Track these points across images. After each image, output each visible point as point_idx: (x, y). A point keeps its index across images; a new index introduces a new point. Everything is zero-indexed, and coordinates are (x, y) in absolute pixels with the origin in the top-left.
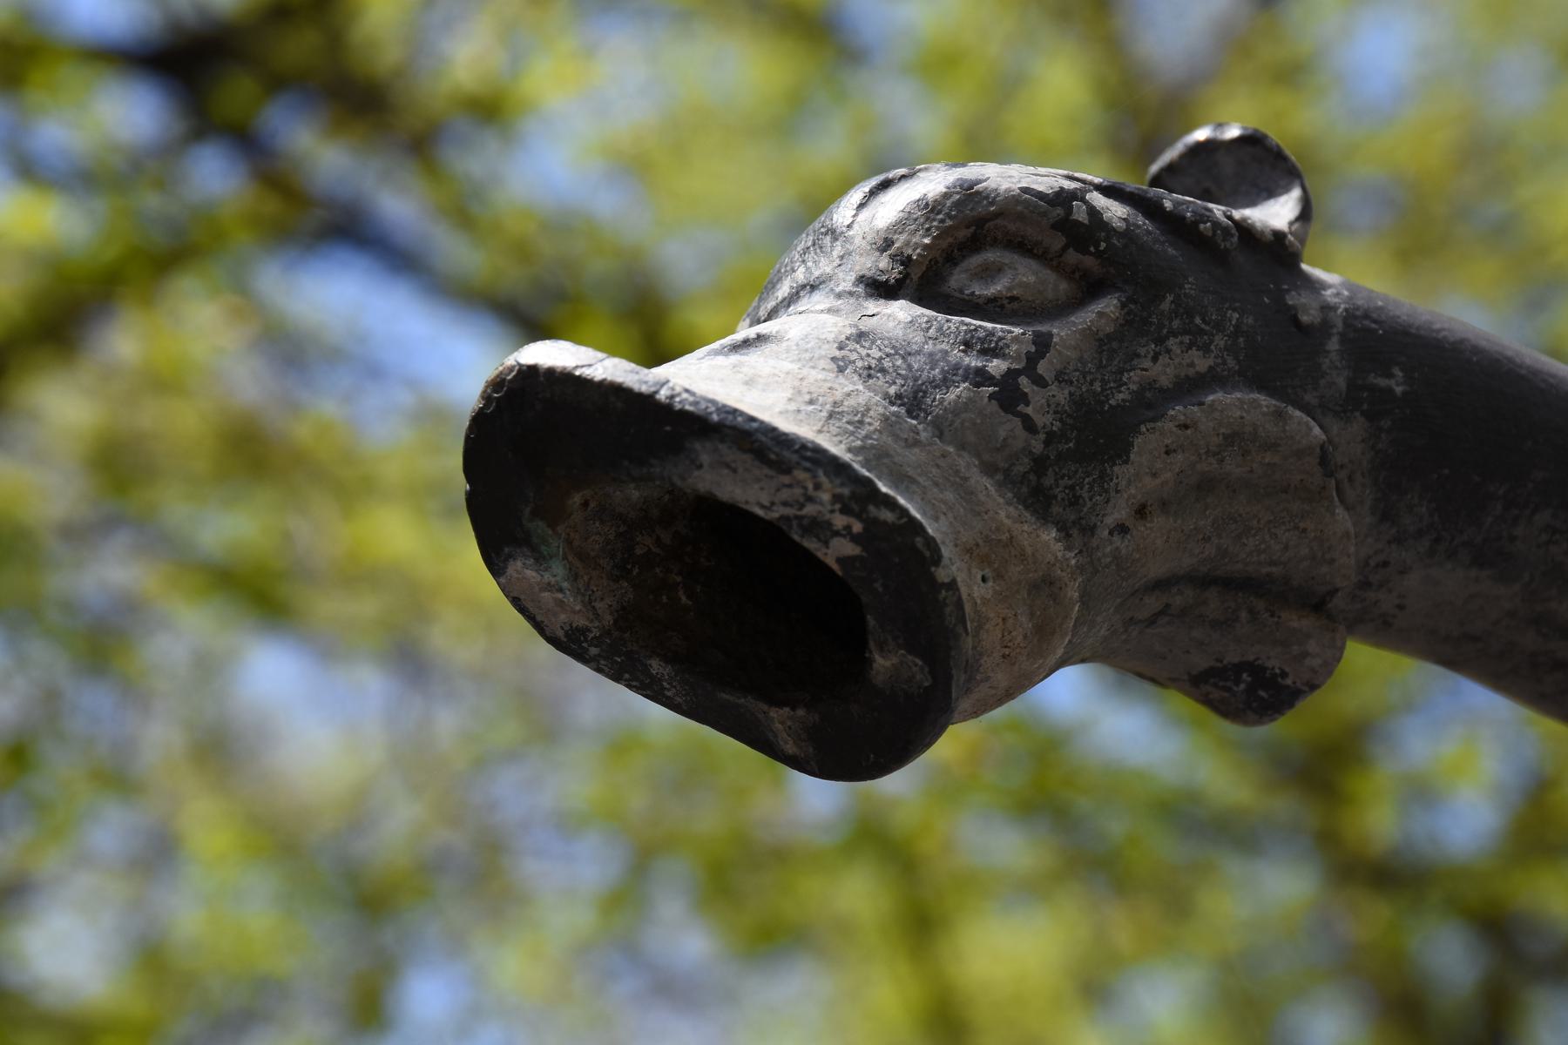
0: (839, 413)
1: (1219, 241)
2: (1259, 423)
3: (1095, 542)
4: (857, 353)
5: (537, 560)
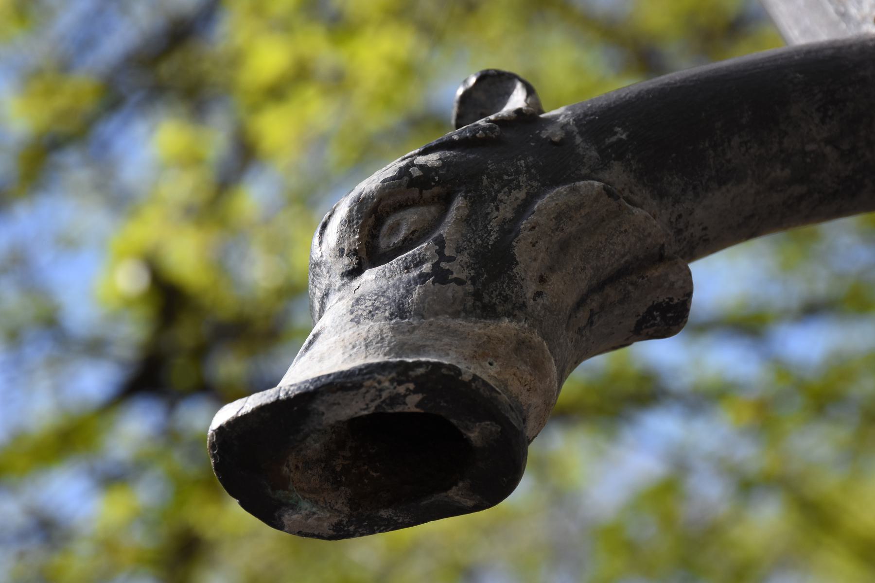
0: (369, 342)
1: (491, 135)
2: (566, 201)
3: (530, 310)
4: (361, 310)
5: (292, 508)
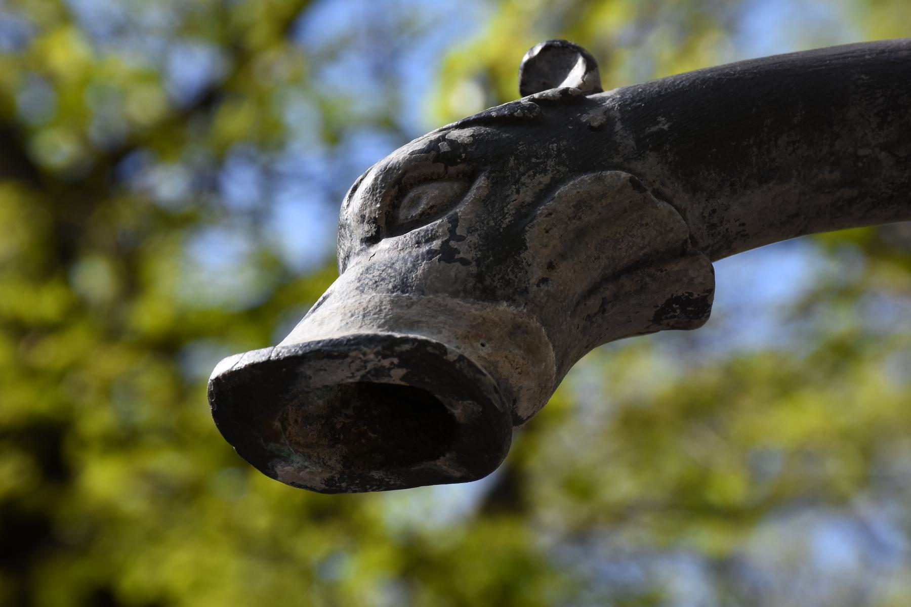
0: (367, 313)
1: (529, 115)
3: (531, 295)
4: (368, 279)
5: (284, 461)
